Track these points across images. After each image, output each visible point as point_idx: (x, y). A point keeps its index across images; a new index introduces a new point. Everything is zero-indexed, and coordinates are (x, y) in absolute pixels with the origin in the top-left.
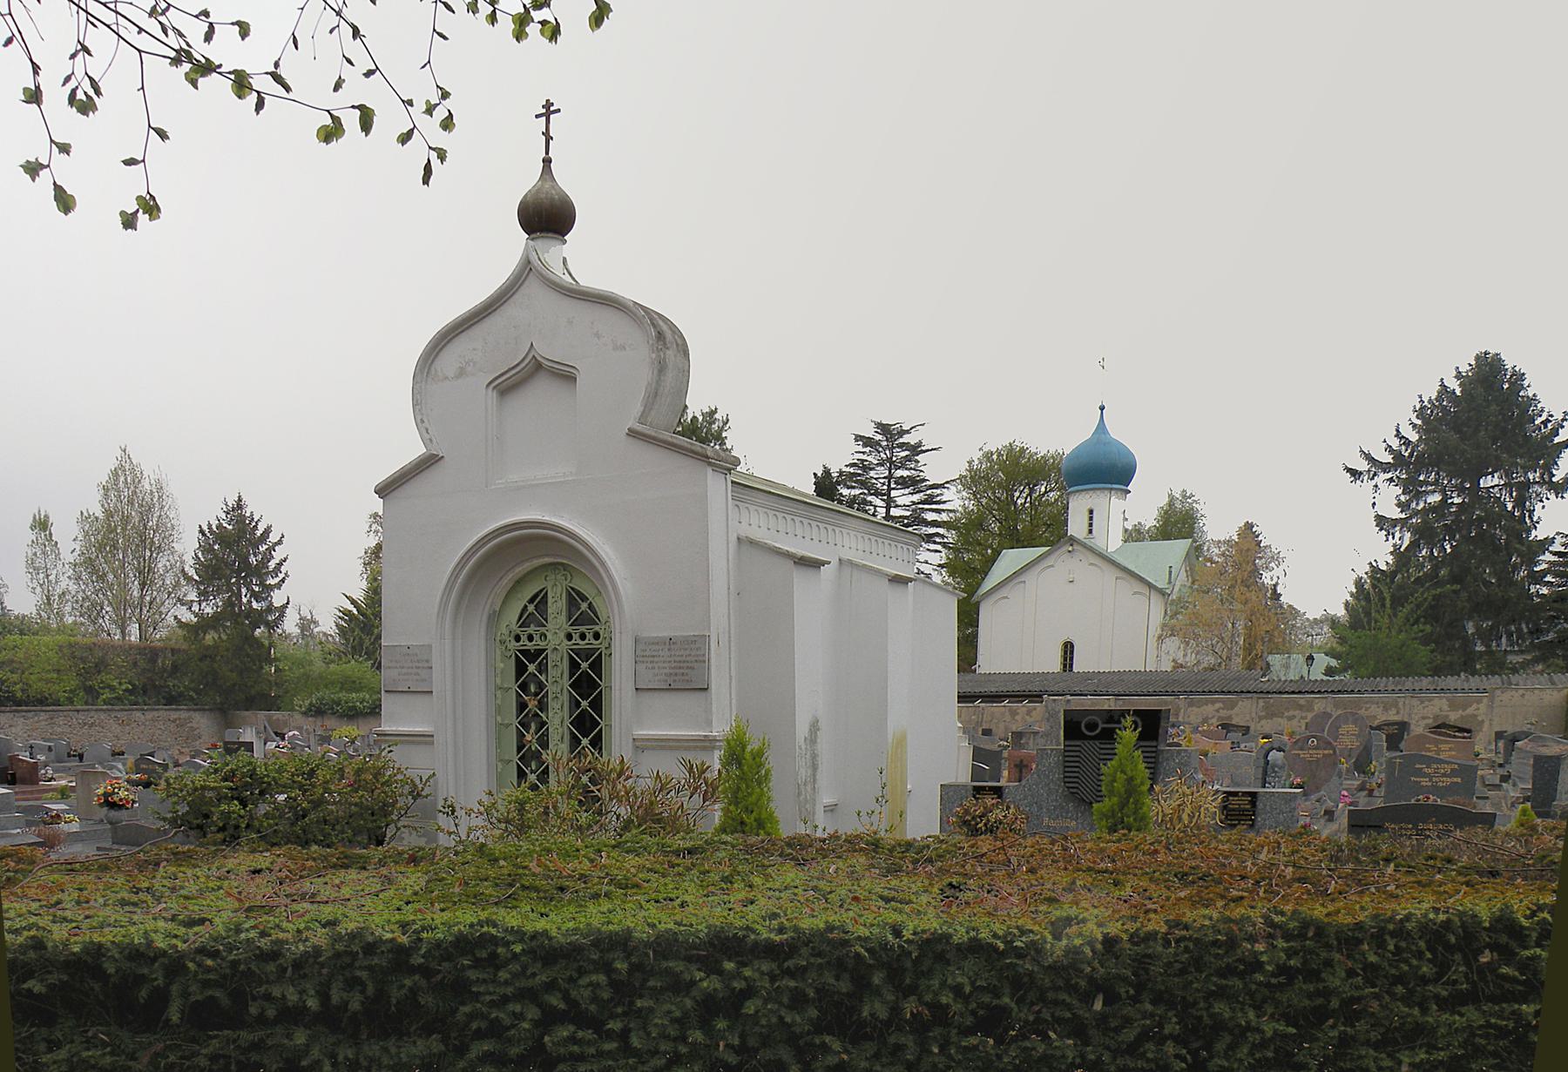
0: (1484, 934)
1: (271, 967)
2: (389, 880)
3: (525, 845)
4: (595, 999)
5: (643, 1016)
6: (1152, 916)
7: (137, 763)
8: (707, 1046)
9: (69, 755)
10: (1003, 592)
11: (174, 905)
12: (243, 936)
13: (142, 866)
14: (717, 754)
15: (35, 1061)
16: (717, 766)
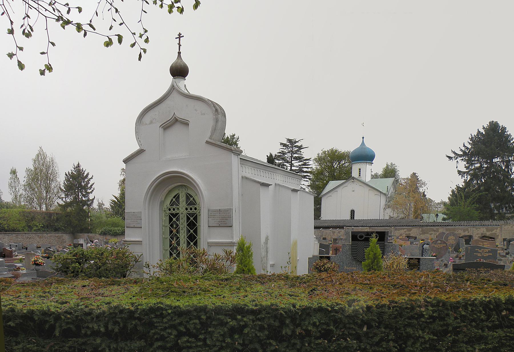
0: (503, 305)
1: (89, 318)
2: (128, 289)
3: (172, 278)
4: (195, 328)
5: (211, 334)
6: (384, 299)
7: (45, 251)
8: (232, 343)
9: (23, 248)
10: (330, 194)
11: (57, 297)
12: (80, 307)
13: (46, 284)
14: (235, 247)
15: (12, 349)
16: (235, 251)
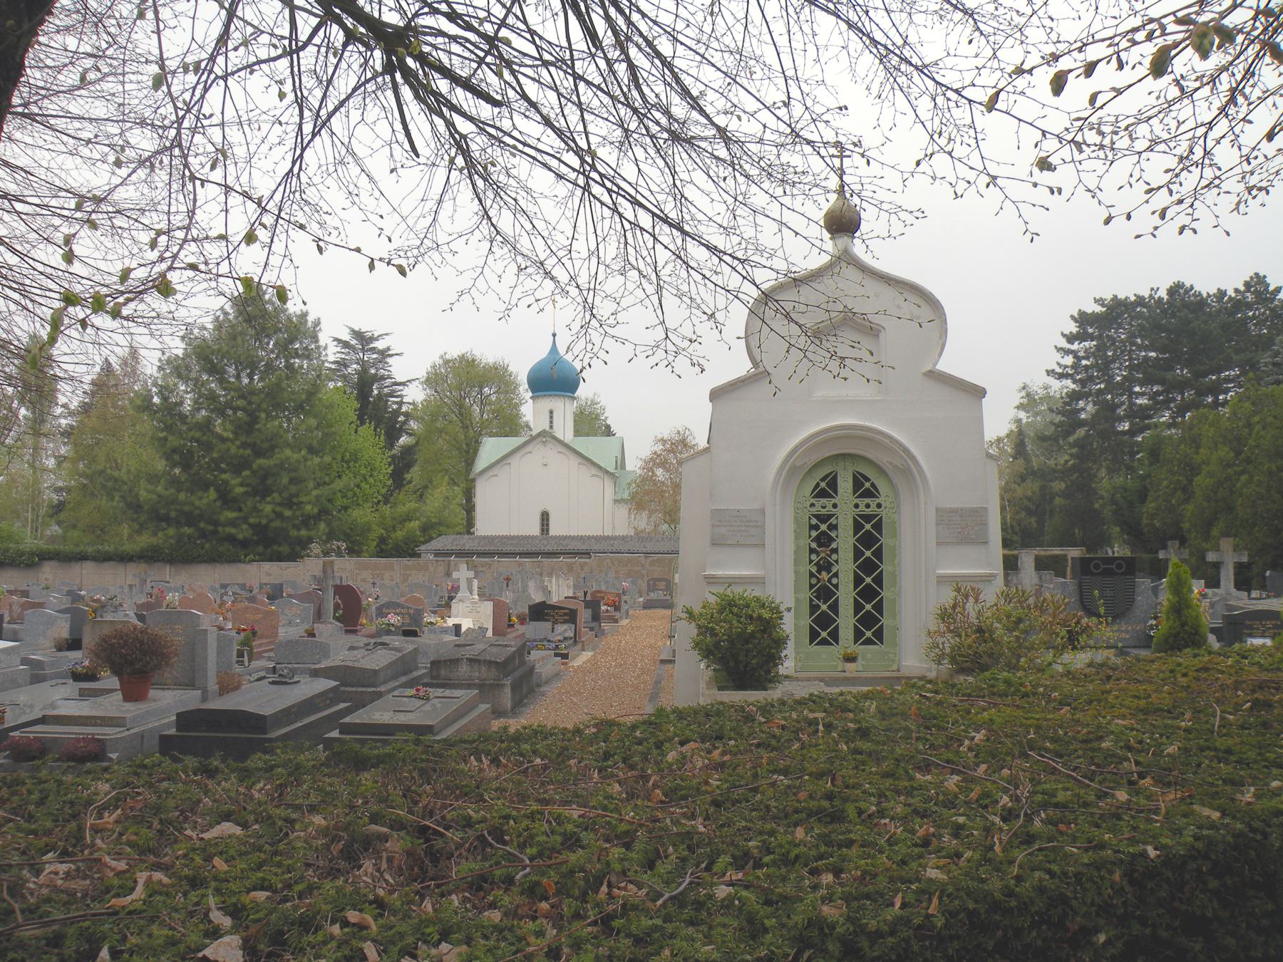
10: (491, 473)
